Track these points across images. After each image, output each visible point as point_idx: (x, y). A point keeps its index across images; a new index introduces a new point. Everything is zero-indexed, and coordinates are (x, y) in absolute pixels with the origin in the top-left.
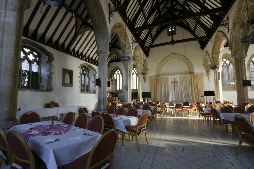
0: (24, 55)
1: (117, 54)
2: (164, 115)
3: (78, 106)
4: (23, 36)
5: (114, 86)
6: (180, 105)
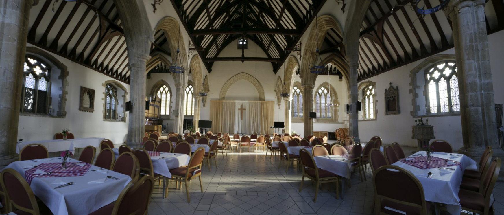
0: (28, 68)
1: (165, 62)
2: (227, 151)
3: (100, 139)
4: (28, 42)
5: (157, 109)
6: (247, 137)
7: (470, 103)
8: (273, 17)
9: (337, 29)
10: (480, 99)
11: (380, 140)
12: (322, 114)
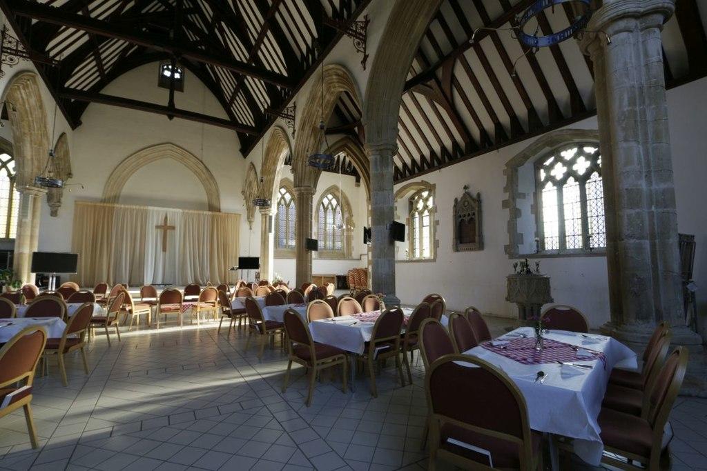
7: (626, 230)
8: (246, 41)
9: (355, 95)
10: (647, 223)
11: (442, 303)
12: (328, 243)
